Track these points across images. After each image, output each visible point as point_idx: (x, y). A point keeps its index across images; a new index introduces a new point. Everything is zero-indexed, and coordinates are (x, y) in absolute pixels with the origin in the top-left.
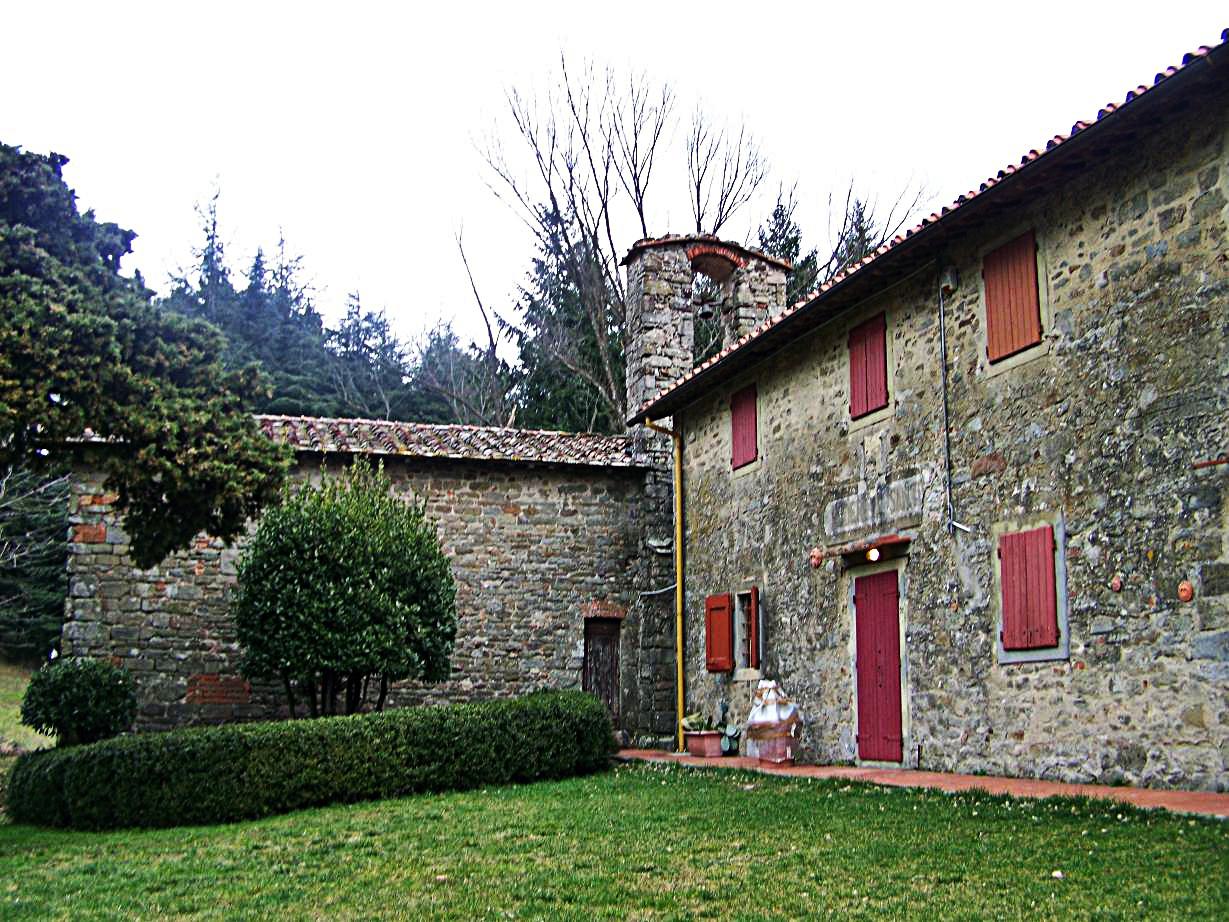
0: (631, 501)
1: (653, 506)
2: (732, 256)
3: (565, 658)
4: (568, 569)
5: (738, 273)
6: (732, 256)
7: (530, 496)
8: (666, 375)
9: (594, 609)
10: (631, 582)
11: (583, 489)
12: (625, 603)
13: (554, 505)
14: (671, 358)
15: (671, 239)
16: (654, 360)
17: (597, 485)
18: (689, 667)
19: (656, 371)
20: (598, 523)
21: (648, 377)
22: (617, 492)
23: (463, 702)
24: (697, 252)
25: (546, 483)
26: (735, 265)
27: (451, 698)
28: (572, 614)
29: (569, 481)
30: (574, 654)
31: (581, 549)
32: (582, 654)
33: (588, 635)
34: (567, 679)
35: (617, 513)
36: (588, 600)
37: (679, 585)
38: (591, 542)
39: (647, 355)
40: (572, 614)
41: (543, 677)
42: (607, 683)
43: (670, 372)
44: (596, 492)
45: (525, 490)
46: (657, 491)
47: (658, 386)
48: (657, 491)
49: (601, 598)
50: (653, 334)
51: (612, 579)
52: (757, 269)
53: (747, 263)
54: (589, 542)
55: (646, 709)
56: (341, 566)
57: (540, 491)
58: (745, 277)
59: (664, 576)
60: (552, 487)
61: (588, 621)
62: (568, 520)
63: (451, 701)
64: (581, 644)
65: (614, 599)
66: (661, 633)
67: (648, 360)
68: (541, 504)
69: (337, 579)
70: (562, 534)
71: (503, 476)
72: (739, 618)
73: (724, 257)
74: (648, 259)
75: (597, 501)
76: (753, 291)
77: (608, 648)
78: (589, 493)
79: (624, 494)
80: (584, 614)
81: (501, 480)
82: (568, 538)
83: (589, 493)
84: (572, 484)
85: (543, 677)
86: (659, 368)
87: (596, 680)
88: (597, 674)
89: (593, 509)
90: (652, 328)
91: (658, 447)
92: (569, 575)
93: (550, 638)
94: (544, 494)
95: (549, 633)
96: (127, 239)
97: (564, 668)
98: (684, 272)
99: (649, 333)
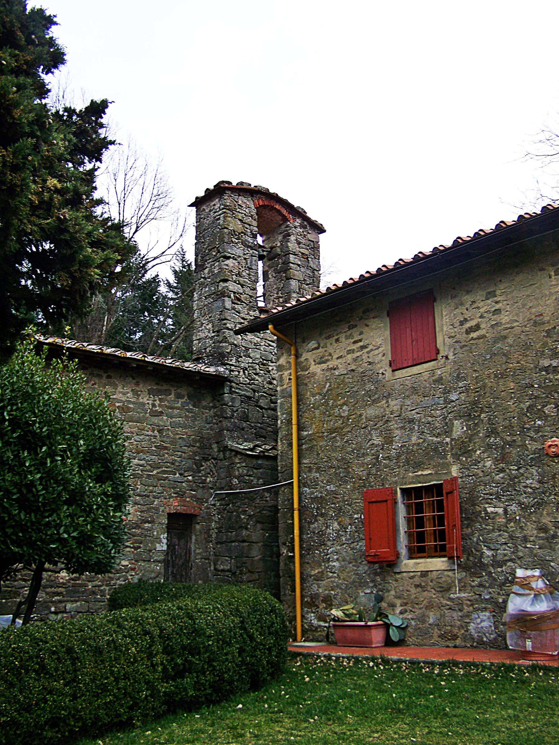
0: (205, 408)
1: (229, 414)
2: (284, 212)
3: (150, 551)
4: (154, 467)
5: (288, 226)
6: (284, 212)
7: (124, 394)
8: (239, 300)
9: (175, 505)
10: (204, 482)
11: (168, 393)
12: (200, 501)
13: (143, 404)
14: (242, 286)
15: (245, 186)
16: (232, 286)
17: (179, 391)
18: (308, 559)
19: (232, 295)
20: (179, 425)
21: (226, 299)
22: (195, 399)
23: (58, 594)
24: (261, 203)
25: (137, 384)
26: (285, 220)
27: (48, 590)
28: (157, 509)
29: (157, 384)
30: (158, 547)
31: (166, 448)
32: (165, 548)
33: (170, 529)
34: (152, 571)
35: (194, 418)
36: (171, 497)
37: (295, 480)
38: (173, 442)
39: (226, 281)
40: (157, 509)
41: (133, 569)
42: (182, 575)
43: (243, 297)
44: (179, 396)
45: (120, 389)
46: (233, 400)
47: (234, 309)
48: (233, 400)
49: (181, 495)
50: (230, 262)
51: (190, 478)
52: (302, 226)
53: (294, 220)
54: (172, 443)
55: (160, 609)
56: (34, 433)
57: (132, 390)
58: (293, 231)
59: (250, 476)
60: (144, 388)
61: (170, 516)
62: (155, 420)
63: (47, 593)
64: (164, 536)
65: (192, 496)
66: (247, 529)
67: (226, 284)
68: (133, 403)
69: (33, 450)
70: (150, 433)
71: (101, 372)
72: (402, 511)
73: (279, 211)
74: (228, 199)
75: (179, 405)
76: (299, 243)
77: (183, 541)
78: (172, 396)
79: (199, 401)
80: (167, 510)
81: (100, 376)
82: (155, 437)
83: (172, 396)
84: (159, 387)
85: (133, 569)
86: (234, 293)
87: (172, 572)
88: (173, 566)
89: (176, 412)
90: (228, 258)
91: (233, 362)
92: (155, 472)
93: (138, 531)
94: (136, 393)
95: (137, 527)
96: (50, 21)
97: (149, 561)
98: (252, 216)
99: (227, 262)
